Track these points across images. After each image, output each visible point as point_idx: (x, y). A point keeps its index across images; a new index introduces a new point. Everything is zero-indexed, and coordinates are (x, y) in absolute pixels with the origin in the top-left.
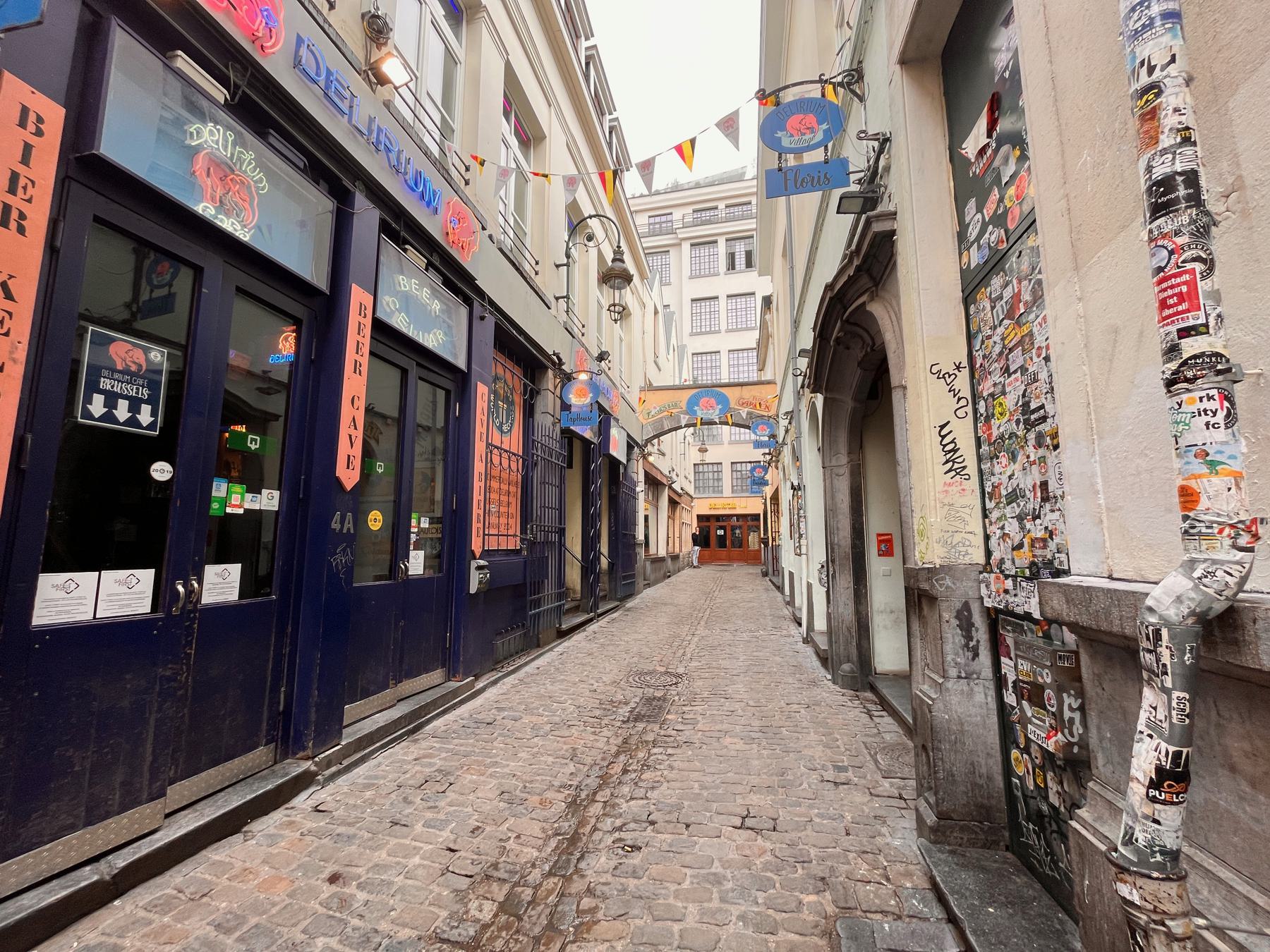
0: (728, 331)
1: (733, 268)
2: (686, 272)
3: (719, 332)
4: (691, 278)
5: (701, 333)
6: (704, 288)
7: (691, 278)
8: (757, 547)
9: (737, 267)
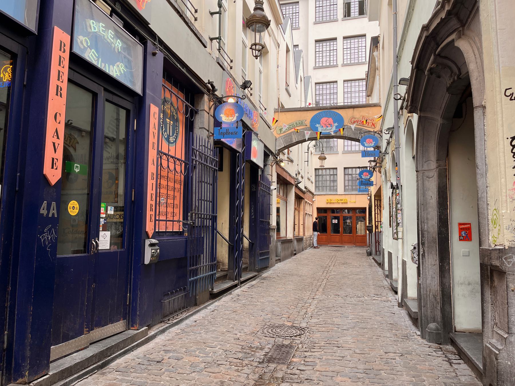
0: (344, 65)
1: (349, 15)
2: (312, 18)
3: (336, 66)
4: (316, 23)
5: (323, 67)
6: (325, 31)
7: (316, 23)
8: (363, 233)
9: (352, 14)
